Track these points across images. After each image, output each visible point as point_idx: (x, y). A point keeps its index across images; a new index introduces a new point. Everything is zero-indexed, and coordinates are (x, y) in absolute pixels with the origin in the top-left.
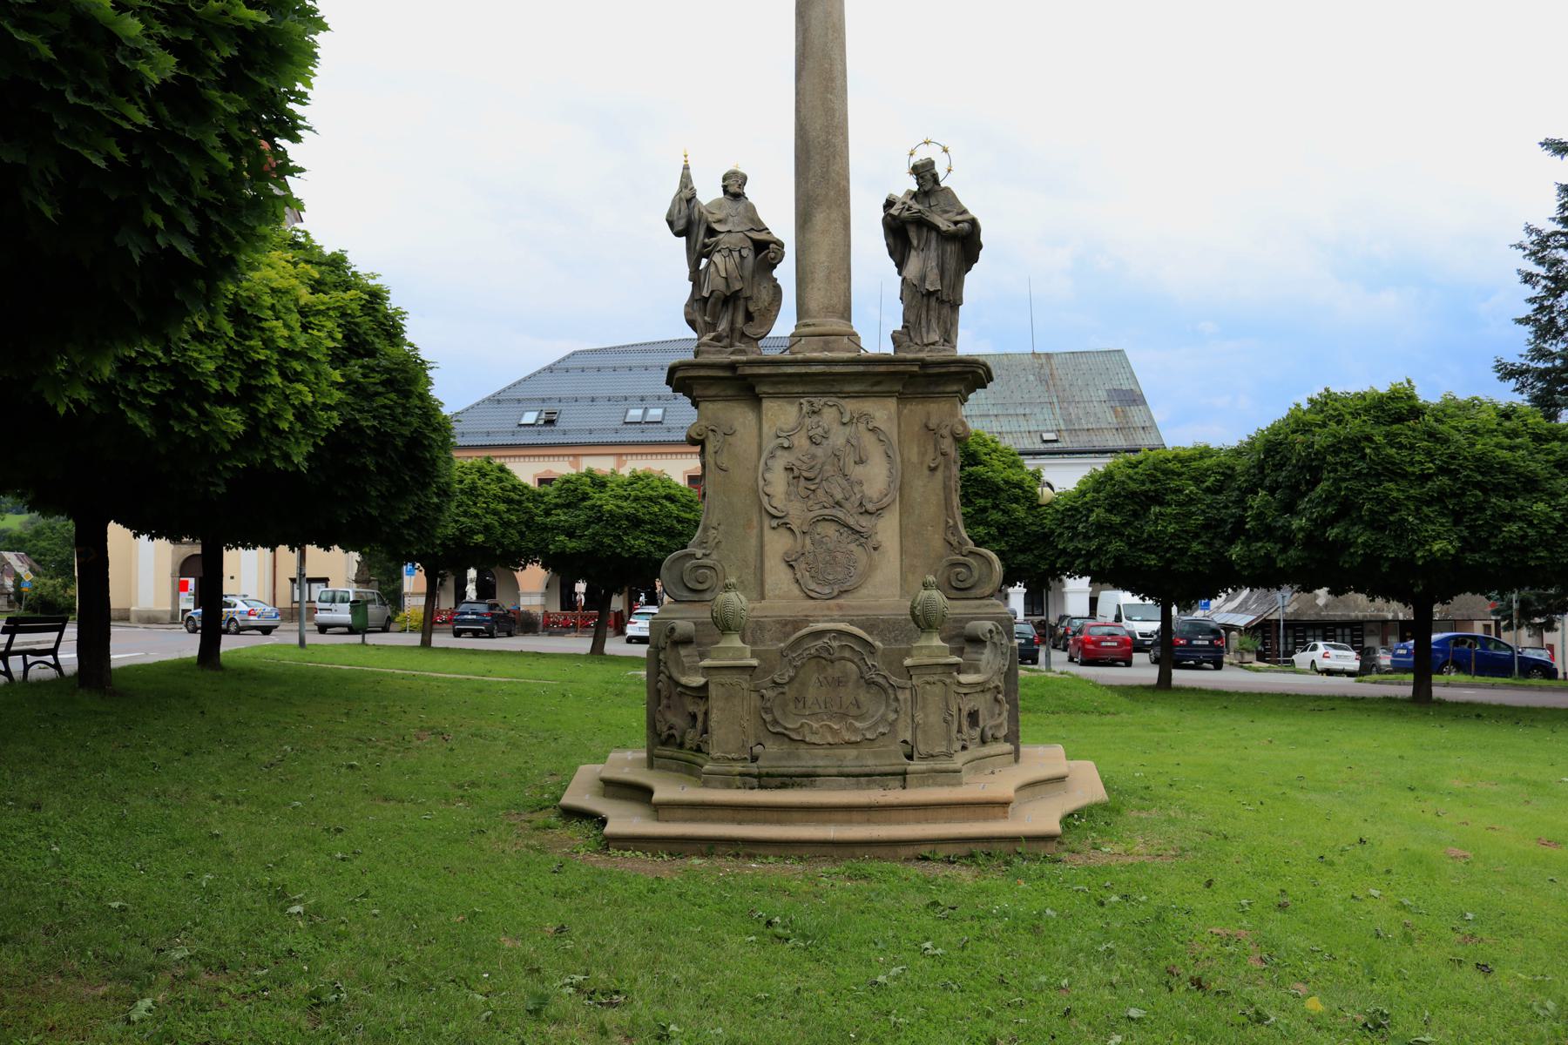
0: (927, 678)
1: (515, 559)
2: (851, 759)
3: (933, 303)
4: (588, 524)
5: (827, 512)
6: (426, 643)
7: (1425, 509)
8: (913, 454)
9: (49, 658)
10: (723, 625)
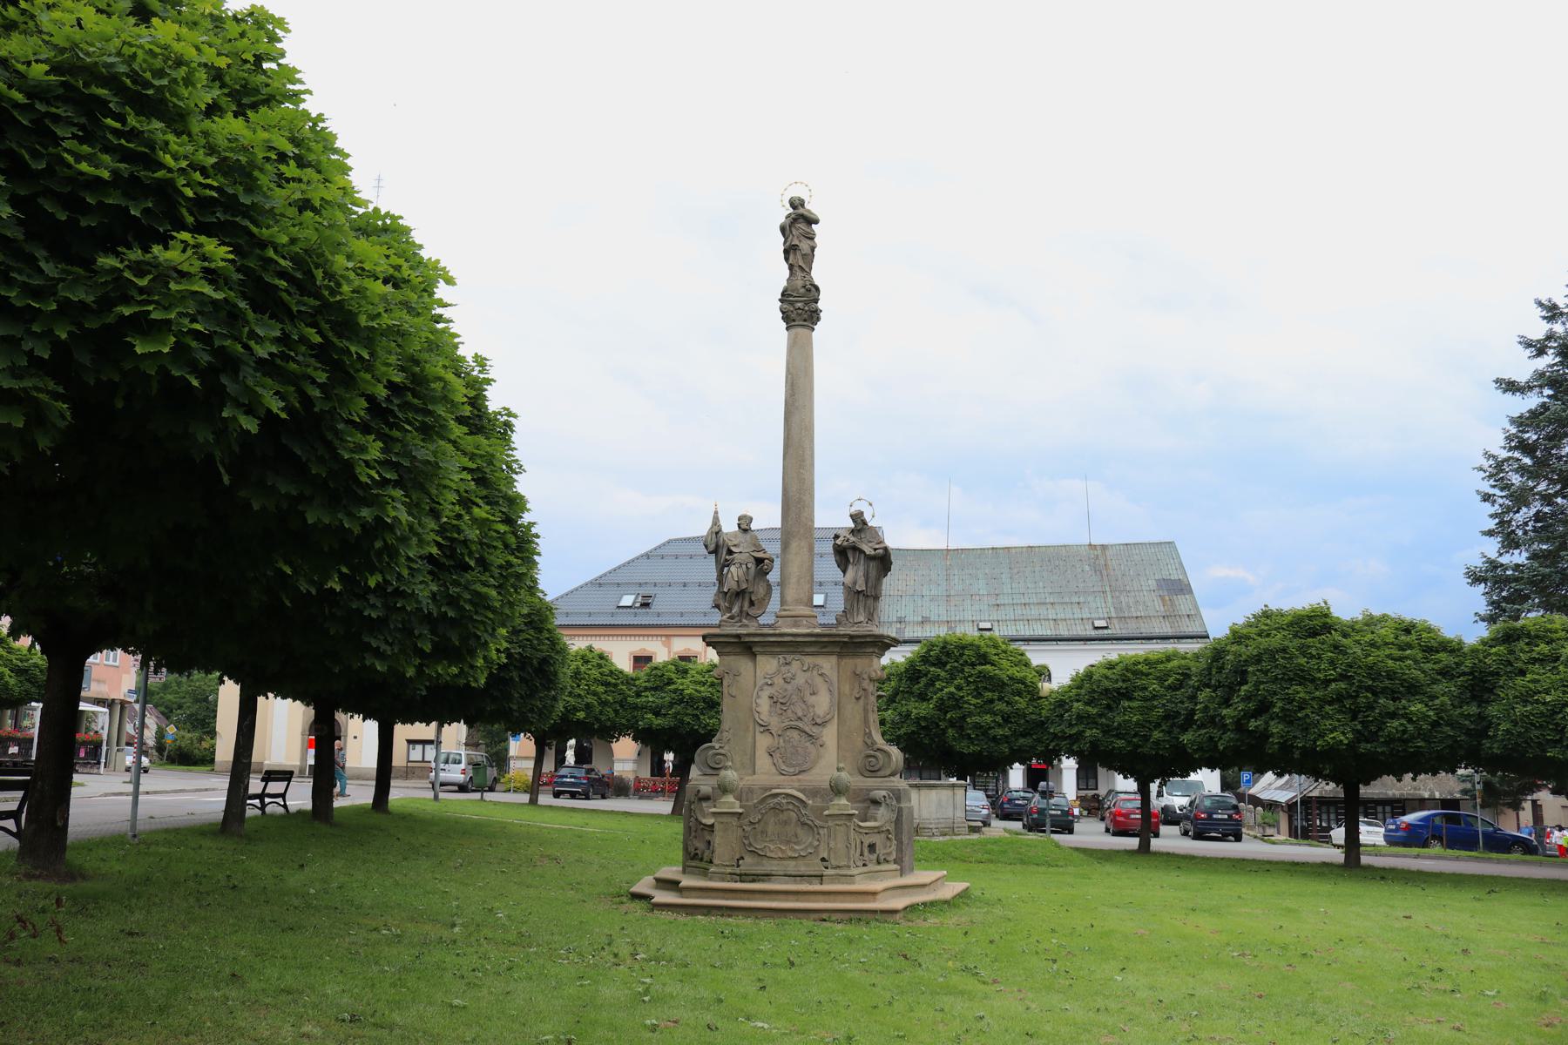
1: (609, 733)
2: (791, 867)
3: (864, 597)
4: (671, 705)
6: (533, 801)
7: (1327, 708)
8: (846, 688)
9: (280, 800)
10: (724, 789)
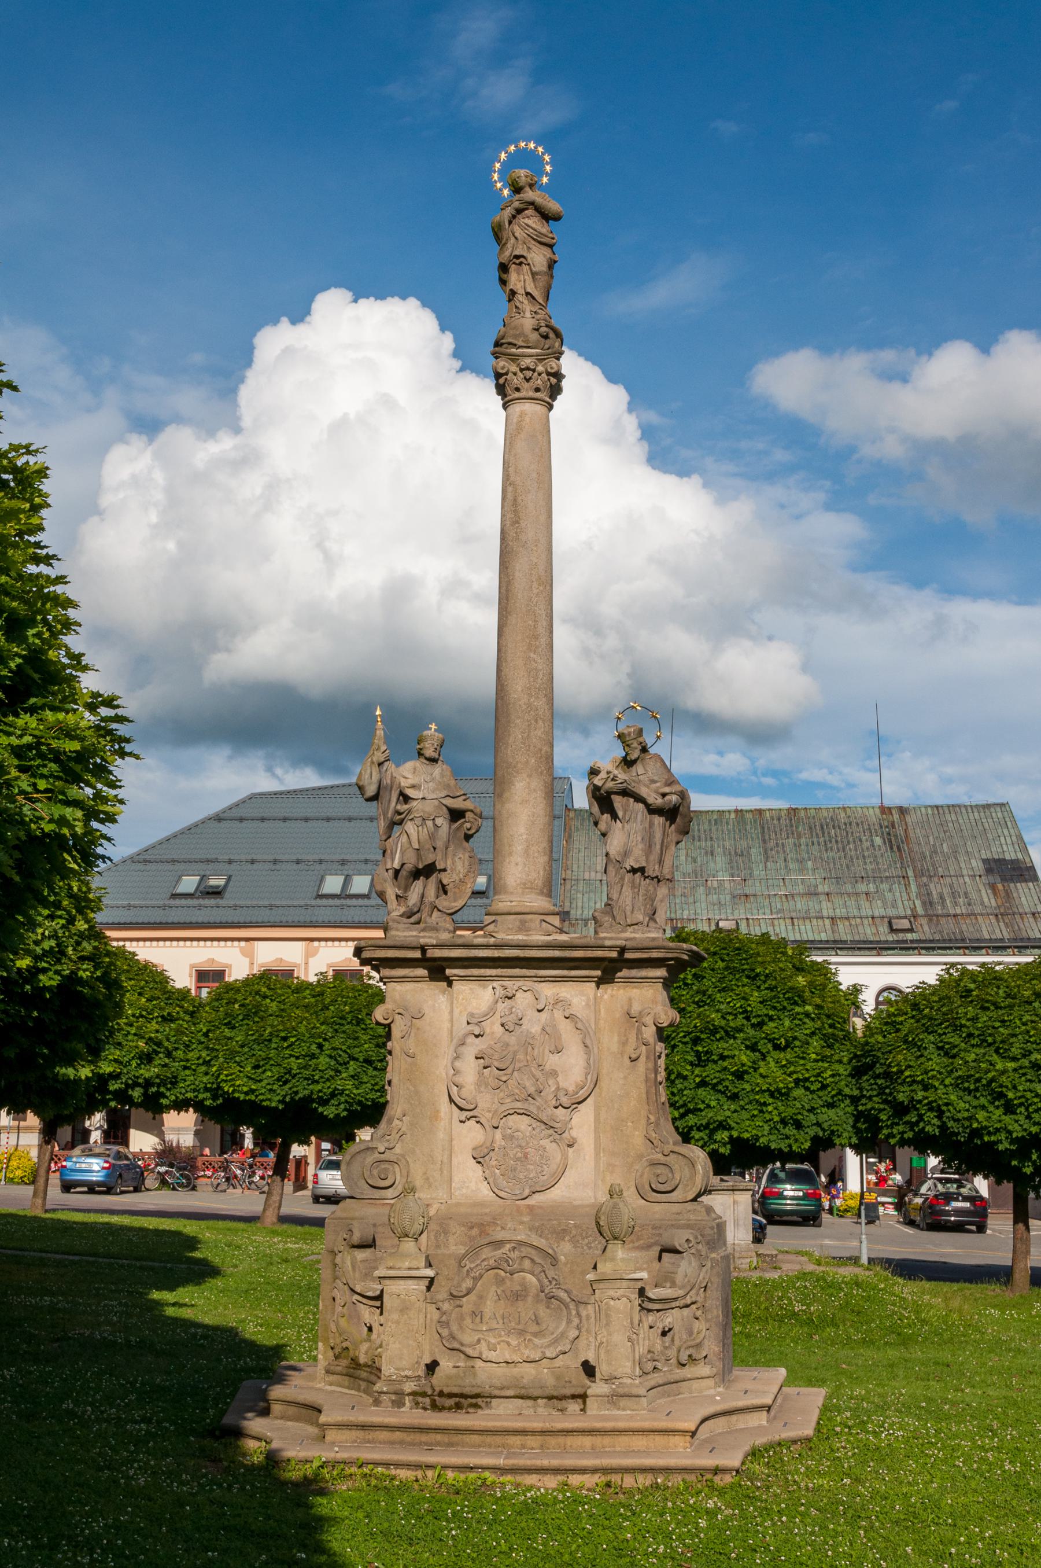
0: (611, 1293)
5: (518, 1105)
